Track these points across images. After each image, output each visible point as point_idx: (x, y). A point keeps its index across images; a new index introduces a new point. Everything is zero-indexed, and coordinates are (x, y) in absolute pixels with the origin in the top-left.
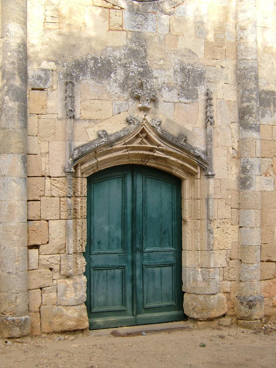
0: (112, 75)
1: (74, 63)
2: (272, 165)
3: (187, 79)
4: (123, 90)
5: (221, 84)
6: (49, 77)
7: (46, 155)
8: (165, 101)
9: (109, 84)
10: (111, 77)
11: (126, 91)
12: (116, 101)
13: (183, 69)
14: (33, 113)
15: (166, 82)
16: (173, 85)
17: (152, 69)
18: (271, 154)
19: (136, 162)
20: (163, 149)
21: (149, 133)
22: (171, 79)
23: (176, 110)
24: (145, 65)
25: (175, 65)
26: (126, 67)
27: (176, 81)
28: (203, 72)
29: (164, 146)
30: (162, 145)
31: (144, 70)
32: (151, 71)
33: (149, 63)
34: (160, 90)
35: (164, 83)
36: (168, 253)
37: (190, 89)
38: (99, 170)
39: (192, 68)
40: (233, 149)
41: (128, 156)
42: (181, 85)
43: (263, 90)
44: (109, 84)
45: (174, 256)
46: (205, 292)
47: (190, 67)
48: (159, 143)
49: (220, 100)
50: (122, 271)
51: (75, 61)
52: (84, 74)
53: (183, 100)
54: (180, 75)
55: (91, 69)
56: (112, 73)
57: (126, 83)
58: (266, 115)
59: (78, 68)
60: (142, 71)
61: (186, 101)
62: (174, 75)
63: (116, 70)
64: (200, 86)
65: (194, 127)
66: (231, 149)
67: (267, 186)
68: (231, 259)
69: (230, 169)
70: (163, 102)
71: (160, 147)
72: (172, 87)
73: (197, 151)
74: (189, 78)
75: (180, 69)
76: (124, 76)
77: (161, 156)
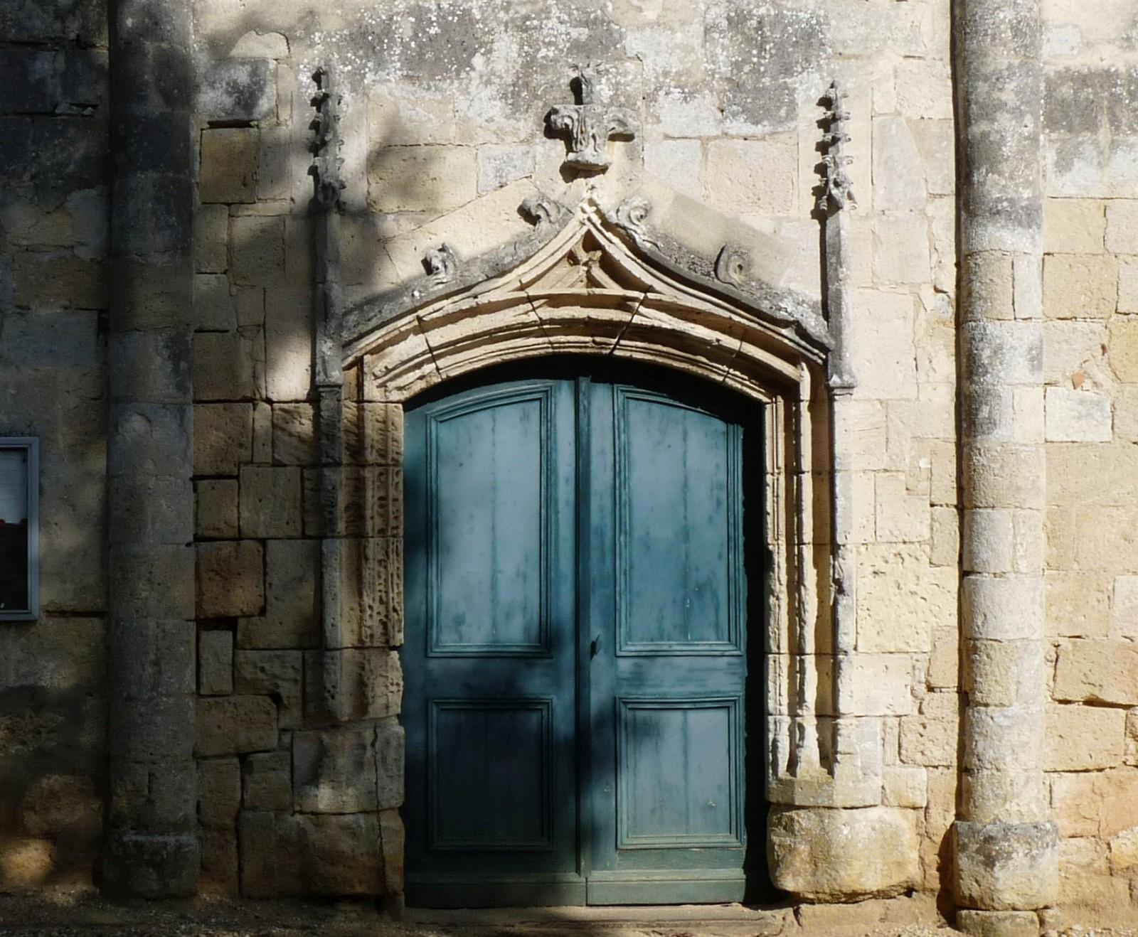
0: (478, 61)
1: (345, 32)
2: (1103, 348)
3: (755, 52)
4: (515, 107)
5: (885, 64)
6: (265, 84)
7: (259, 332)
8: (667, 137)
9: (466, 92)
10: (473, 69)
11: (527, 111)
12: (489, 145)
13: (737, 22)
14: (212, 201)
15: (674, 70)
16: (699, 76)
17: (623, 30)
18: (1101, 306)
19: (652, 354)
20: (660, 300)
21: (610, 249)
22: (693, 57)
23: (710, 164)
24: (596, 18)
25: (708, 8)
26: (526, 31)
27: (713, 62)
28: (818, 23)
29: (666, 291)
30: (658, 285)
31: (592, 33)
32: (616, 36)
33: (610, 9)
34: (650, 98)
35: (666, 74)
36: (708, 662)
37: (763, 88)
38: (444, 376)
39: (772, 13)
40: (937, 290)
41: (541, 329)
42: (729, 75)
43: (1068, 70)
44: (466, 92)
45: (734, 674)
46: (820, 801)
47: (768, 10)
48: (647, 279)
49: (881, 118)
50: (542, 717)
51: (350, 24)
52: (381, 65)
53: (739, 126)
54: (726, 42)
55: (405, 46)
56: (478, 55)
57: (527, 85)
58: (1078, 164)
59: (361, 48)
60: (583, 38)
61: (749, 129)
62: (706, 41)
63: (492, 42)
64: (805, 74)
65: (779, 221)
66: (927, 293)
67: (1083, 423)
68: (931, 689)
69: (924, 363)
70: (661, 137)
71: (650, 295)
72: (696, 84)
73: (787, 304)
74: (761, 48)
75: (729, 19)
76: (520, 60)
77: (657, 323)
